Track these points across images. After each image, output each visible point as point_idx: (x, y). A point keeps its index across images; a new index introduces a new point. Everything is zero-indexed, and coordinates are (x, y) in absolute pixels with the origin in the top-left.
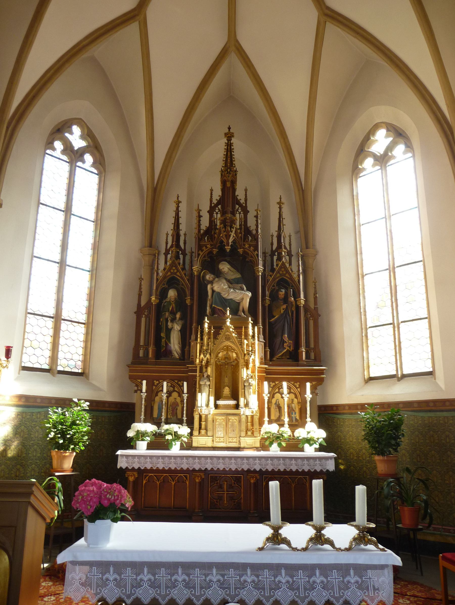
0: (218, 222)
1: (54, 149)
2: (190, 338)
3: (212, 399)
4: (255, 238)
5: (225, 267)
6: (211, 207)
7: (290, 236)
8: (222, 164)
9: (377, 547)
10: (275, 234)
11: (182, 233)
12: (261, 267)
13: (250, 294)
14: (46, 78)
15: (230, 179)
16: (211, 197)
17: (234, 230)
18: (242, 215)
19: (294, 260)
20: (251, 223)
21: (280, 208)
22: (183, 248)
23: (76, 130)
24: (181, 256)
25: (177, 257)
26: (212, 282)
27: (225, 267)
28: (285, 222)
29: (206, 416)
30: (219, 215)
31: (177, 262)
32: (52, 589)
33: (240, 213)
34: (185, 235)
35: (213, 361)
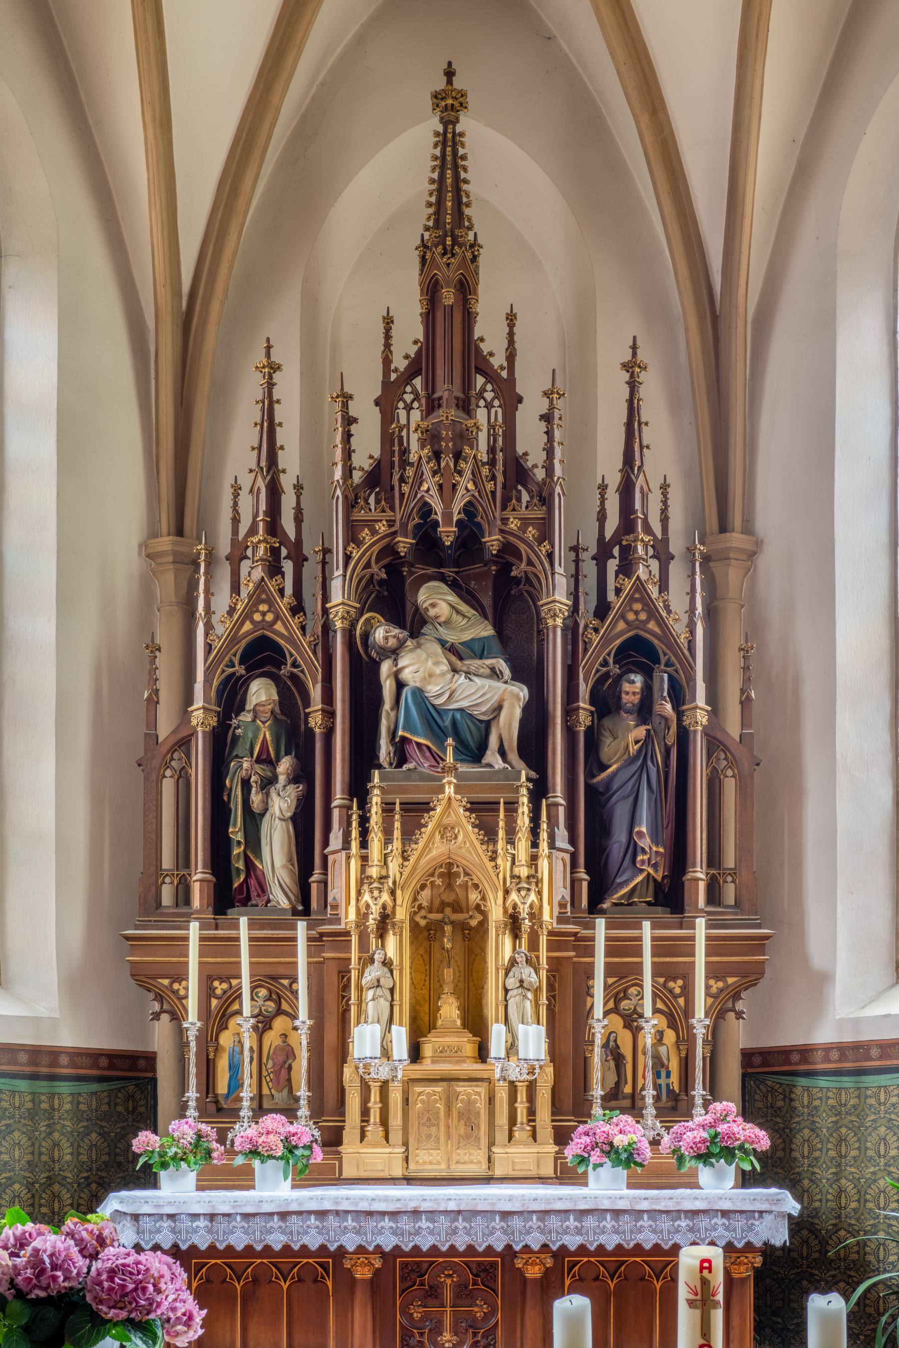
0: (414, 437)
2: (326, 843)
3: (400, 1036)
4: (545, 499)
5: (436, 599)
6: (386, 384)
7: (665, 487)
8: (423, 215)
10: (614, 480)
11: (287, 482)
12: (558, 596)
13: (522, 692)
15: (453, 274)
16: (387, 345)
18: (498, 412)
19: (676, 571)
20: (529, 440)
21: (633, 385)
22: (292, 535)
24: (288, 567)
25: (274, 569)
26: (394, 653)
27: (436, 599)
28: (648, 434)
29: (384, 1086)
30: (416, 415)
31: (272, 585)
33: (489, 406)
34: (298, 488)
35: (401, 914)
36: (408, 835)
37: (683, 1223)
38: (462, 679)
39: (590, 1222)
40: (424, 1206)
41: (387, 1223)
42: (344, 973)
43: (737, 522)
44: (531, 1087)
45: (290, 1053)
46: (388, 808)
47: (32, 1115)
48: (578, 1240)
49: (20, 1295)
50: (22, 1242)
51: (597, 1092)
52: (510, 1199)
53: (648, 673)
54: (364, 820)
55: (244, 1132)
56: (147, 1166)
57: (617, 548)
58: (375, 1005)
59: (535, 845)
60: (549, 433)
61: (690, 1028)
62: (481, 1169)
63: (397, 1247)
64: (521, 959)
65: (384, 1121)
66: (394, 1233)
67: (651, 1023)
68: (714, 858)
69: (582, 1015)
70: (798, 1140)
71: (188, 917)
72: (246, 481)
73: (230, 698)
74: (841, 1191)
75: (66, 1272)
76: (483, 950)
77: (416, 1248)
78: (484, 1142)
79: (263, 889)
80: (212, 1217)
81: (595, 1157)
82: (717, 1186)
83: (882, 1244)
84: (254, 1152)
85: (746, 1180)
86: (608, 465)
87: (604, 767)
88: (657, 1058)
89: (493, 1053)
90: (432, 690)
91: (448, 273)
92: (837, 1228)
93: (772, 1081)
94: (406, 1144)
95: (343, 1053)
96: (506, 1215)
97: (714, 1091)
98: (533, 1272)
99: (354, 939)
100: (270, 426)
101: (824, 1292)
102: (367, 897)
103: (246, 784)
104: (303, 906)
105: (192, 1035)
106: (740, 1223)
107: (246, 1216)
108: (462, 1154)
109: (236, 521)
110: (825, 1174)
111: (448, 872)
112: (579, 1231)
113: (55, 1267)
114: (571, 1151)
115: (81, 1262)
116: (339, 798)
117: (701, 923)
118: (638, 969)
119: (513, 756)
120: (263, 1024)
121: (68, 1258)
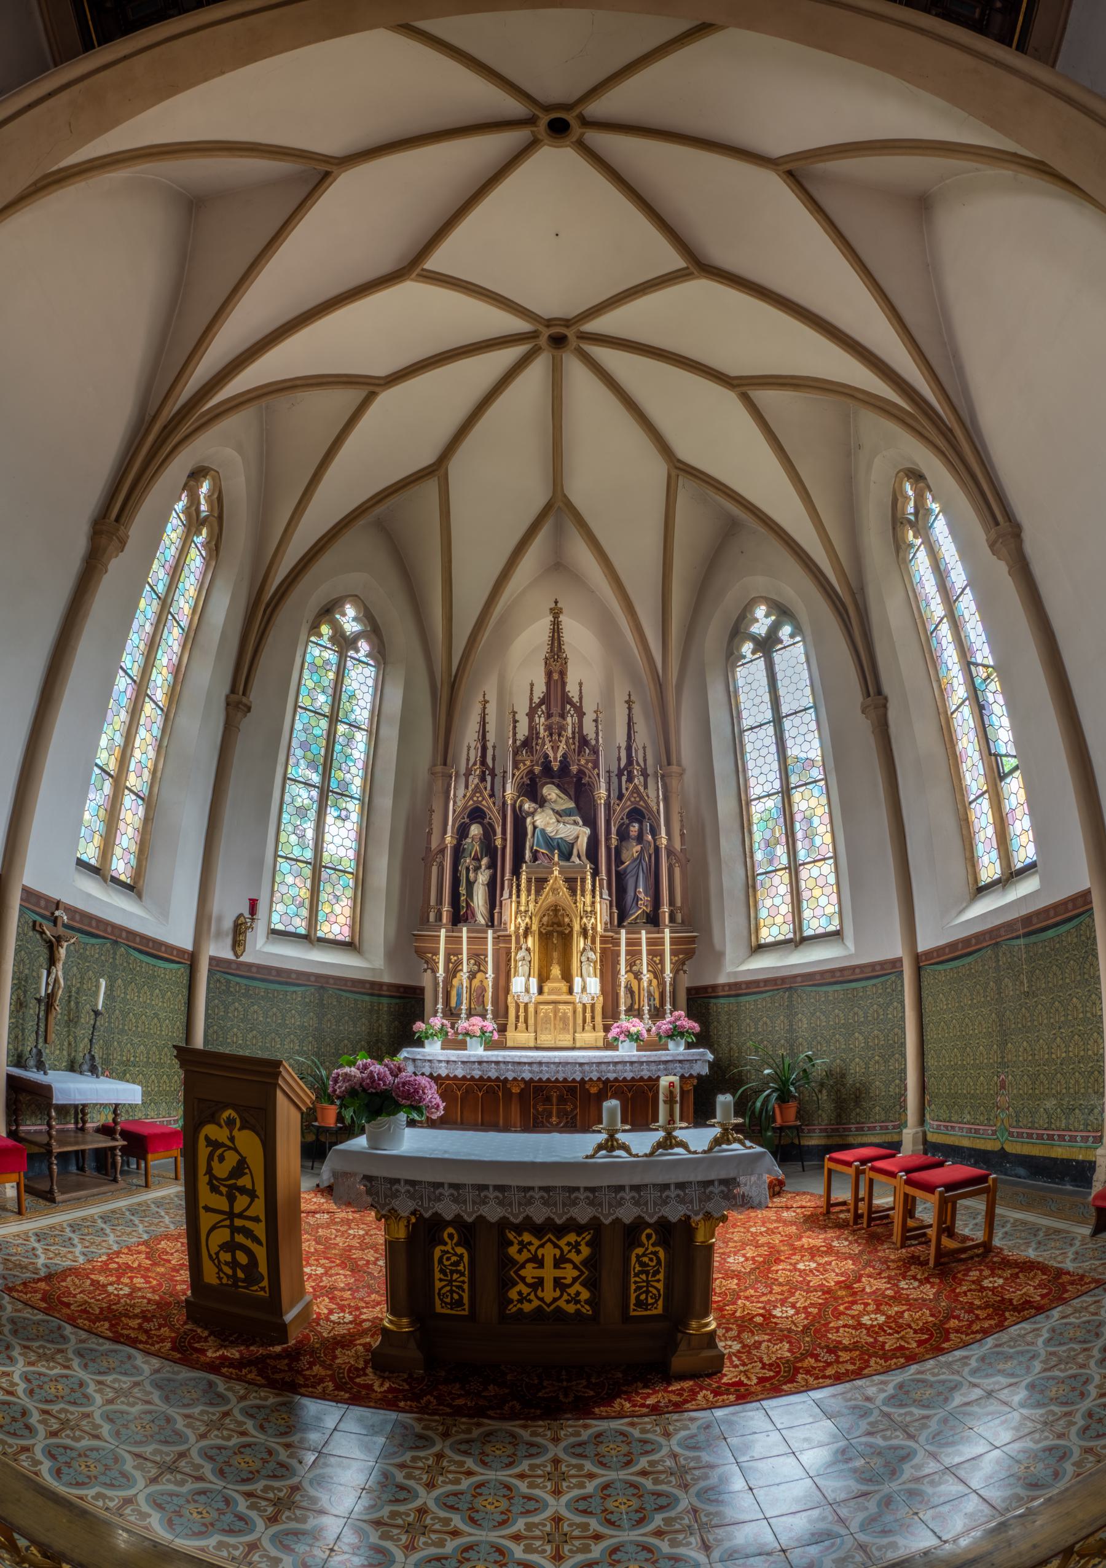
0: (542, 728)
1: (320, 636)
2: (501, 895)
3: (534, 982)
4: (595, 751)
5: (550, 792)
6: (531, 707)
7: (644, 748)
8: (546, 648)
9: (743, 1144)
10: (624, 745)
11: (490, 745)
12: (602, 792)
13: (587, 831)
14: (317, 548)
15: (558, 668)
16: (531, 694)
17: (564, 740)
18: (576, 718)
19: (650, 781)
20: (589, 729)
21: (630, 709)
22: (491, 766)
23: (350, 611)
24: (489, 778)
26: (533, 814)
27: (550, 792)
28: (636, 728)
29: (526, 1005)
30: (542, 720)
31: (482, 786)
32: (325, 1206)
33: (572, 716)
34: (494, 747)
35: (535, 927)
36: (538, 892)
37: (662, 1067)
38: (562, 825)
39: (620, 1067)
40: (544, 1060)
41: (527, 1067)
42: (509, 953)
43: (674, 761)
44: (593, 1006)
45: (483, 989)
46: (529, 880)
47: (371, 1011)
48: (615, 1075)
49: (364, 1090)
50: (365, 1067)
51: (623, 1008)
52: (583, 1057)
53: (641, 823)
54: (518, 886)
55: (463, 1024)
56: (419, 1038)
57: (626, 771)
58: (523, 968)
59: (594, 897)
60: (597, 727)
61: (664, 978)
62: (569, 1044)
63: (531, 1079)
64: (588, 948)
65: (526, 1021)
66: (530, 1072)
67: (646, 976)
68: (672, 903)
69: (616, 973)
70: (712, 1027)
71: (440, 927)
72: (473, 744)
73: (462, 832)
74: (731, 1049)
75: (384, 1082)
76: (571, 944)
77: (540, 1079)
78: (571, 1031)
79: (473, 915)
80: (448, 1062)
81: (622, 1038)
82: (677, 1049)
83: (749, 1071)
84: (467, 1034)
85: (689, 1046)
86: (621, 739)
87: (623, 863)
88: (649, 992)
89: (575, 990)
90: (549, 830)
91: (556, 667)
92: (729, 1065)
93: (700, 1001)
94: (536, 1032)
95: (507, 990)
96: (581, 1064)
97: (675, 1007)
98: (594, 1090)
99: (513, 938)
100: (483, 723)
101: (723, 1094)
102: (519, 920)
103: (468, 869)
104: (491, 923)
105: (441, 980)
106: (687, 1066)
107: (463, 1062)
108: (561, 1037)
109: (468, 760)
110: (724, 1042)
111: (555, 909)
112: (614, 1072)
113: (379, 1079)
114: (610, 1036)
115: (390, 1078)
116: (507, 876)
117: (667, 931)
118: (640, 952)
119: (584, 858)
120: (472, 976)
121: (385, 1076)
